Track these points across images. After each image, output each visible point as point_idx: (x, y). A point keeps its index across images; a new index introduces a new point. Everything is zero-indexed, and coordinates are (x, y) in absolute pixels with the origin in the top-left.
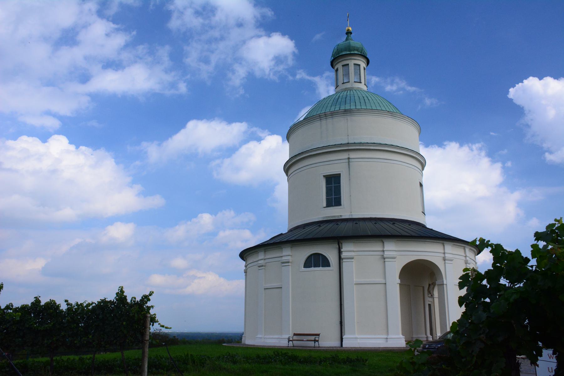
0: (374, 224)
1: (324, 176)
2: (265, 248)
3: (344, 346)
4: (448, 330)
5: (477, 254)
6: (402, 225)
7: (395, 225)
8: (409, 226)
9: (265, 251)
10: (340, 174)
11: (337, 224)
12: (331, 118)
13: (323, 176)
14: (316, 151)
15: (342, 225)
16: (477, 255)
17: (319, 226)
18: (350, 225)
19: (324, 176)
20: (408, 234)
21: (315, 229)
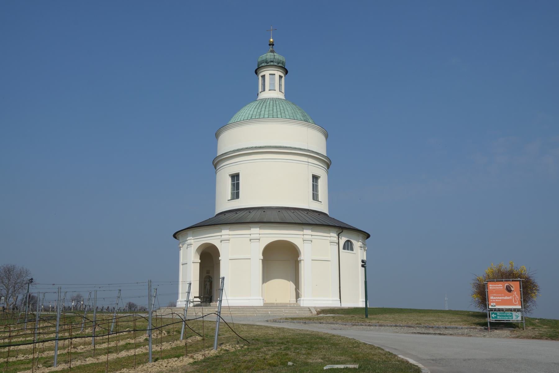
0: (278, 212)
1: (229, 175)
2: (193, 231)
3: (198, 296)
4: (182, 248)
5: (366, 238)
6: (312, 214)
7: (308, 214)
8: (319, 216)
9: (193, 233)
10: (239, 173)
11: (250, 212)
12: (307, 128)
13: (229, 176)
14: (311, 153)
15: (253, 213)
16: (367, 239)
17: (236, 213)
18: (259, 213)
19: (229, 175)
20: (334, 225)
21: (233, 215)
